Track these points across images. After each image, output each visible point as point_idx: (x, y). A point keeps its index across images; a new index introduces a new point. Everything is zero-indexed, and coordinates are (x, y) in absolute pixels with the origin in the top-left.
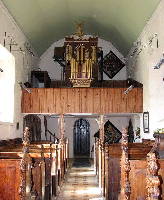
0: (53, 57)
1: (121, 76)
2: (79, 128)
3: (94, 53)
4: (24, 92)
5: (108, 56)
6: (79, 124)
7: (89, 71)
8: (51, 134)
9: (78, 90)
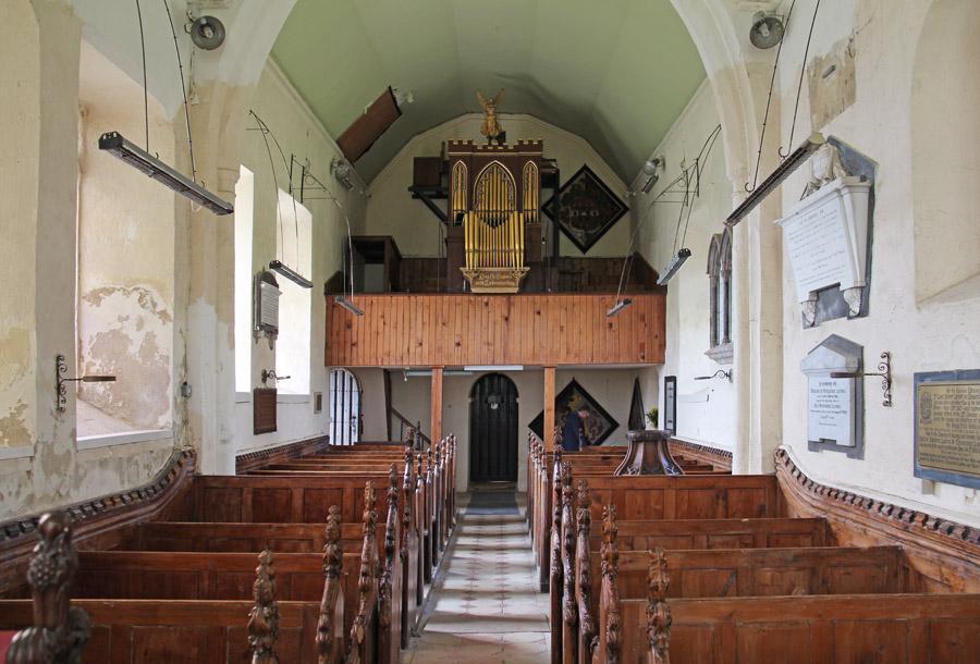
0: (410, 189)
1: (617, 242)
4: (334, 306)
5: (576, 182)
6: (487, 390)
7: (517, 247)
9: (485, 299)
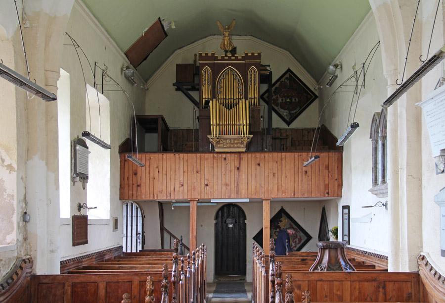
1: (308, 119)
2: (225, 222)
3: (253, 84)
5: (283, 79)
6: (226, 215)
8: (172, 235)
9: (224, 156)
